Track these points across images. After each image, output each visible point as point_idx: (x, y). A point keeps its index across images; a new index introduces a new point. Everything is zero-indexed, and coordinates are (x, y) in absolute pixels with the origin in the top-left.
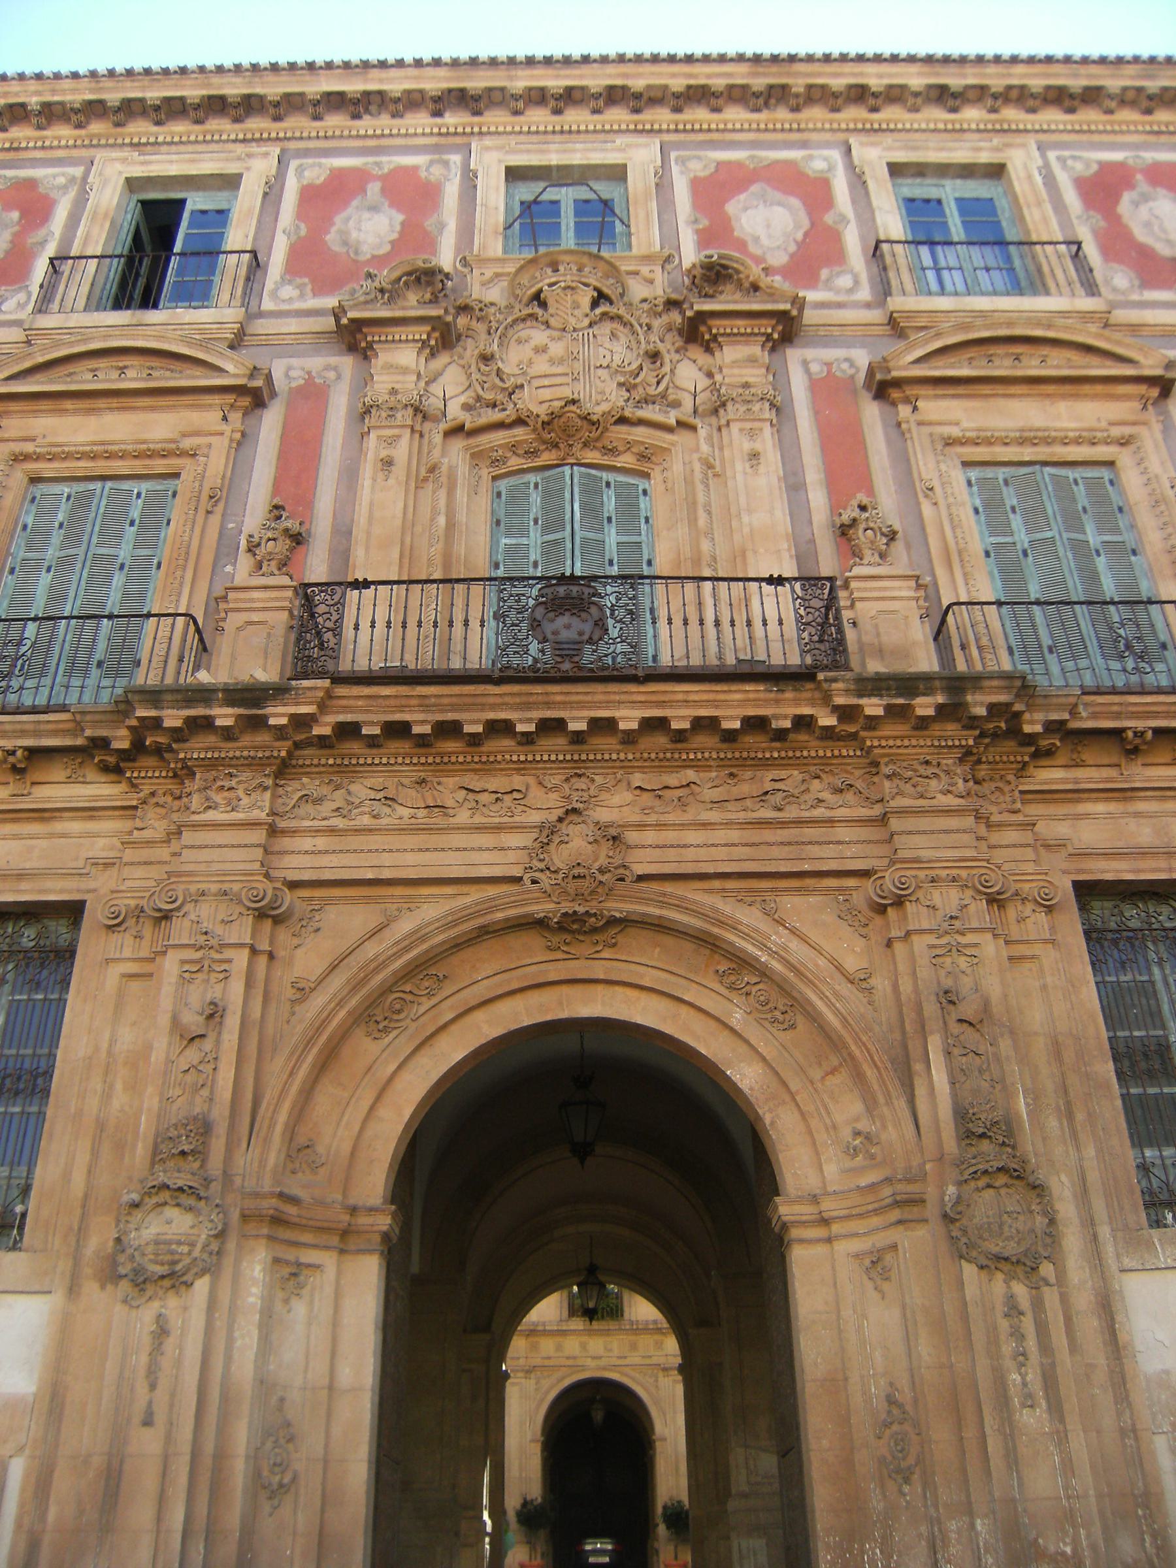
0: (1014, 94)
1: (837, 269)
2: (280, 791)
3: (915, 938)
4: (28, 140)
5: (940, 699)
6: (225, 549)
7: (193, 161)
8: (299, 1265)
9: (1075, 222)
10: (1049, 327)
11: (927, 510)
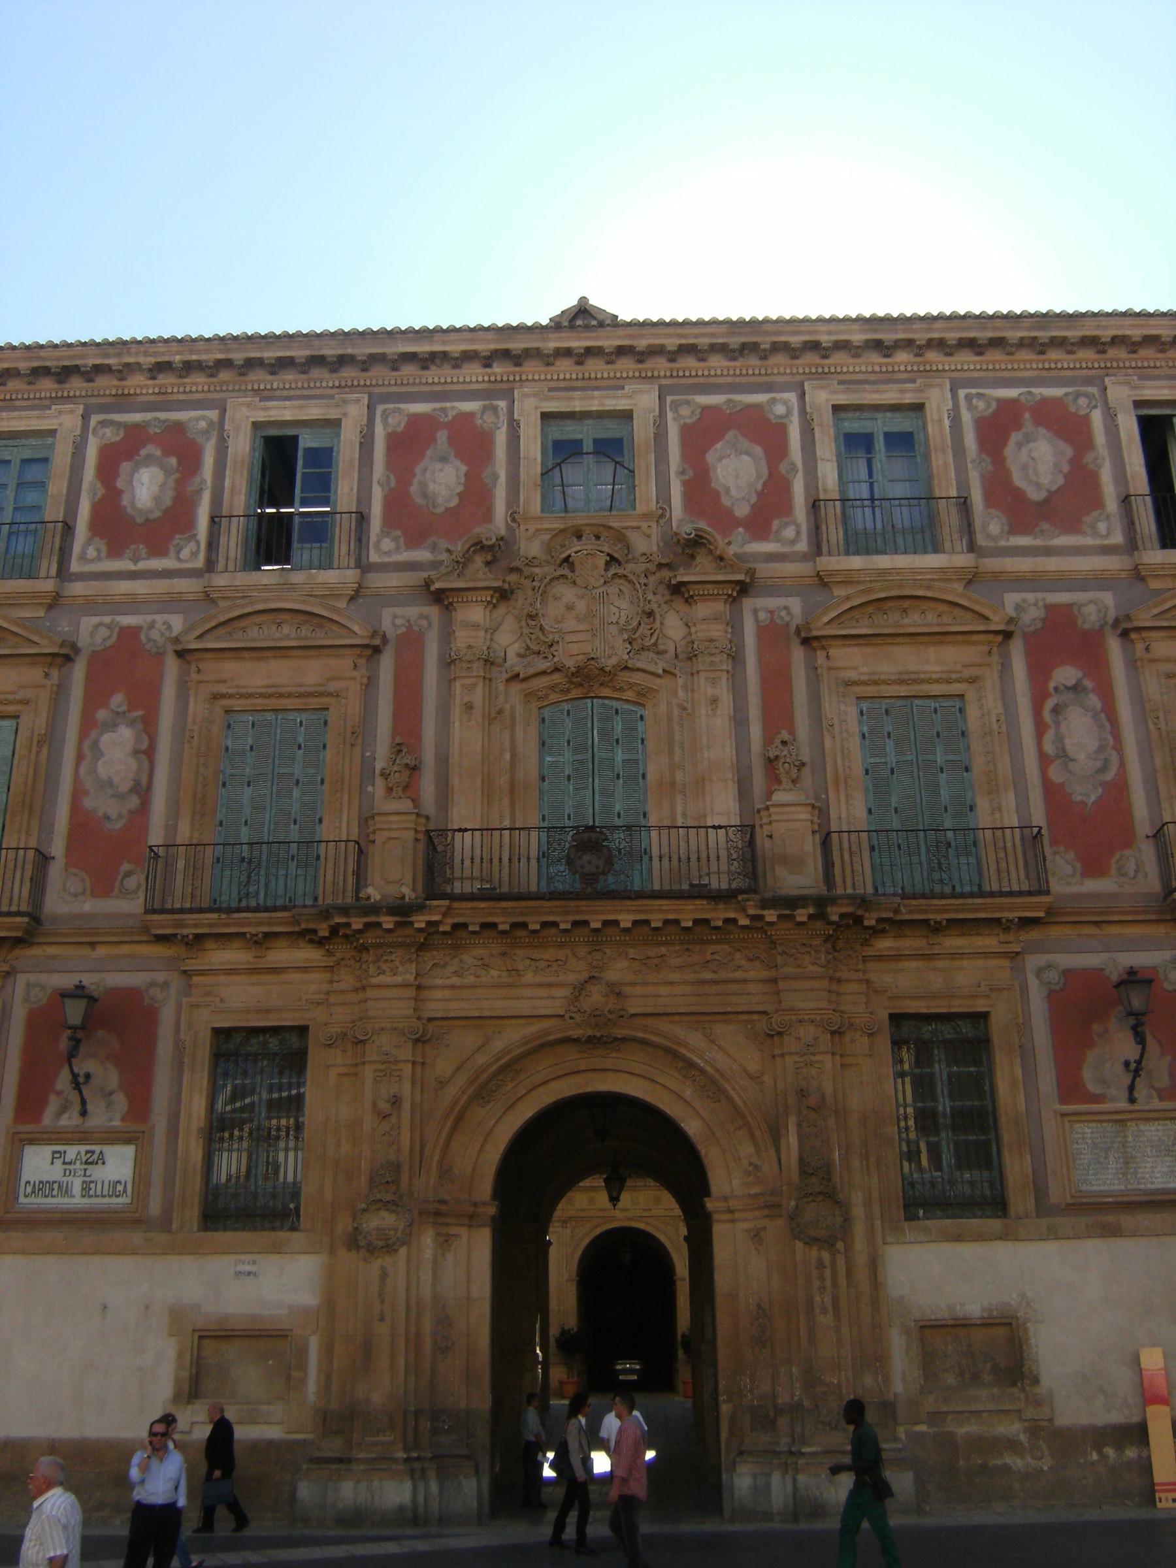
0: (935, 343)
1: (786, 520)
2: (420, 959)
3: (787, 1057)
4: (173, 385)
5: (811, 911)
6: (367, 773)
7: (301, 407)
8: (448, 1235)
9: (970, 466)
10: (928, 588)
11: (828, 743)
